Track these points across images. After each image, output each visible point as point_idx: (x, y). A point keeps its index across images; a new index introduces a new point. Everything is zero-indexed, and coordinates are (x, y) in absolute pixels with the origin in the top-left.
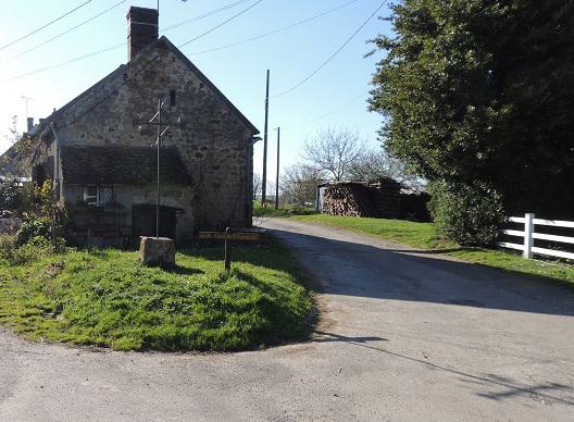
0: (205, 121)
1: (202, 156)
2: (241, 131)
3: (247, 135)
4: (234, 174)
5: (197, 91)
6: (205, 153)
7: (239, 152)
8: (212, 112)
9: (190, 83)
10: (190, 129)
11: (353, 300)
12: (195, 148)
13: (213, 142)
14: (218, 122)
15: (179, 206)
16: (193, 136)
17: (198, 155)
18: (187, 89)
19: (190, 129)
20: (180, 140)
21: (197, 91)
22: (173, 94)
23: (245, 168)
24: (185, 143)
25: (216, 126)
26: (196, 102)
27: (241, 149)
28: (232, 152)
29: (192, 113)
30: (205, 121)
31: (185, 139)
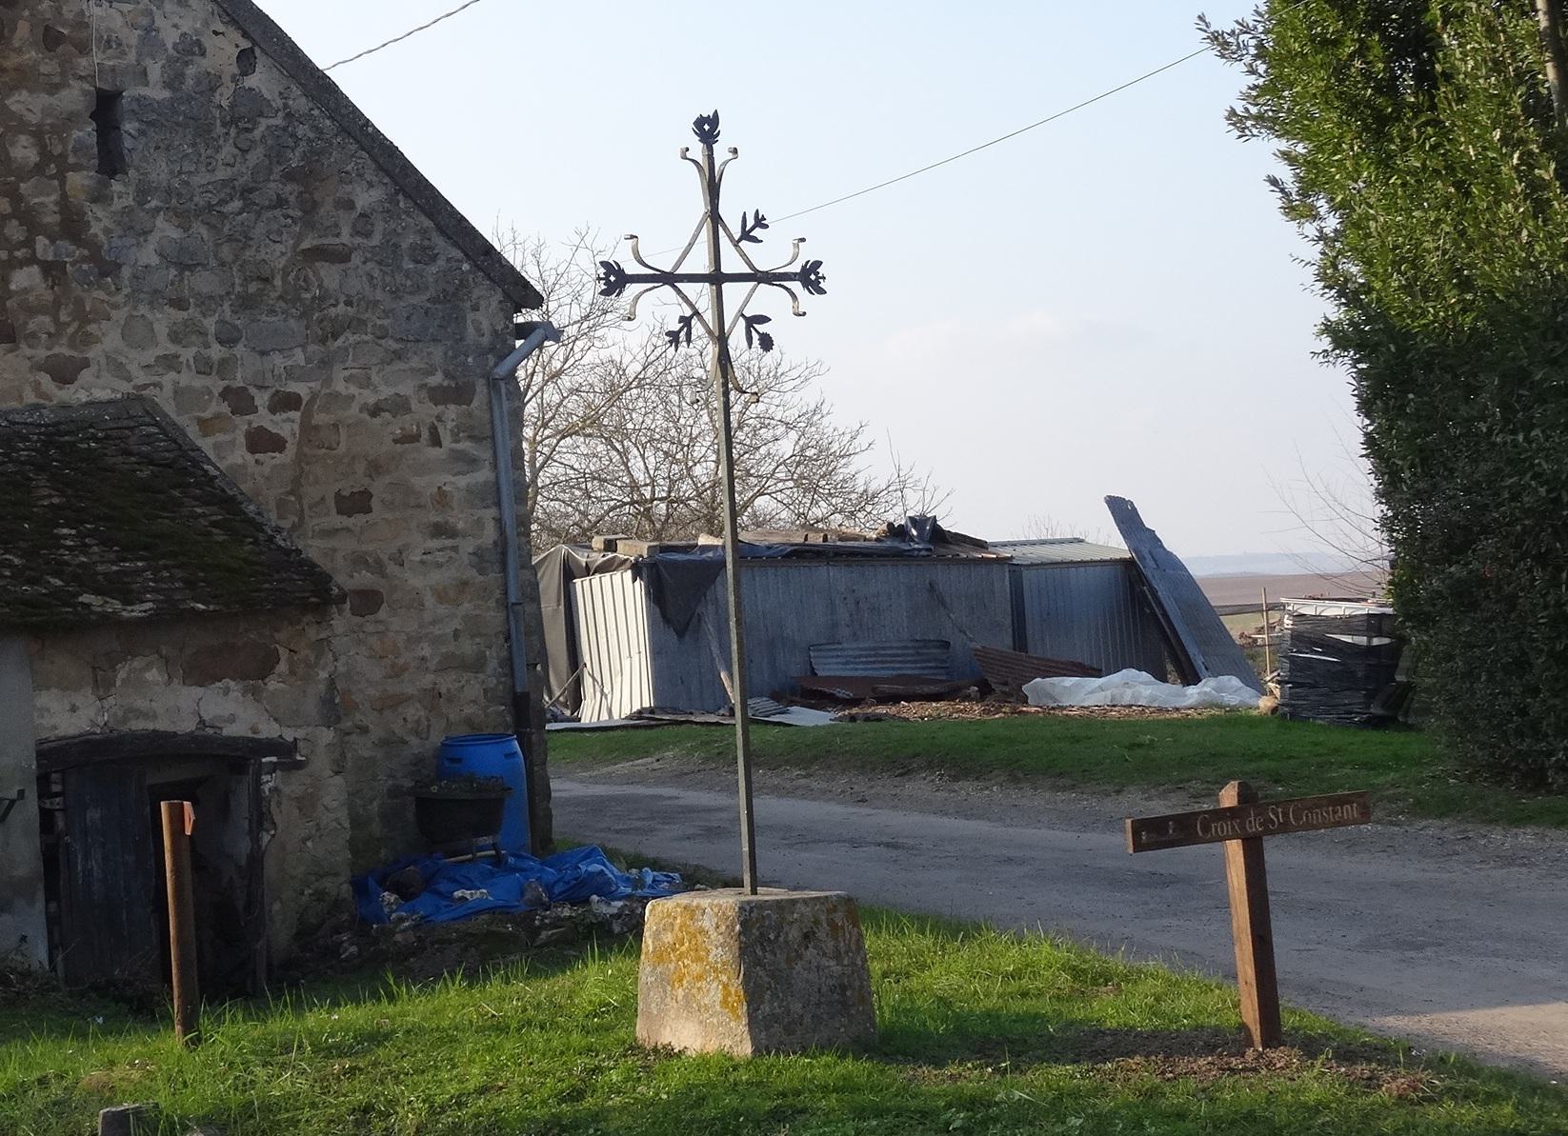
0: (277, 255)
1: (277, 444)
2: (451, 299)
3: (483, 317)
4: (440, 530)
5: (224, 97)
6: (285, 424)
7: (452, 412)
8: (310, 208)
9: (192, 48)
10: (207, 303)
11: (656, 936)
12: (239, 401)
13: (326, 363)
14: (340, 256)
15: (269, 730)
16: (228, 339)
17: (261, 442)
18: (173, 82)
19: (207, 303)
20: (170, 362)
21: (224, 97)
22: (105, 107)
23: (492, 494)
24: (186, 379)
25: (329, 275)
26: (228, 151)
27: (457, 393)
28: (424, 411)
29: (212, 214)
30: (277, 255)
31: (188, 354)
